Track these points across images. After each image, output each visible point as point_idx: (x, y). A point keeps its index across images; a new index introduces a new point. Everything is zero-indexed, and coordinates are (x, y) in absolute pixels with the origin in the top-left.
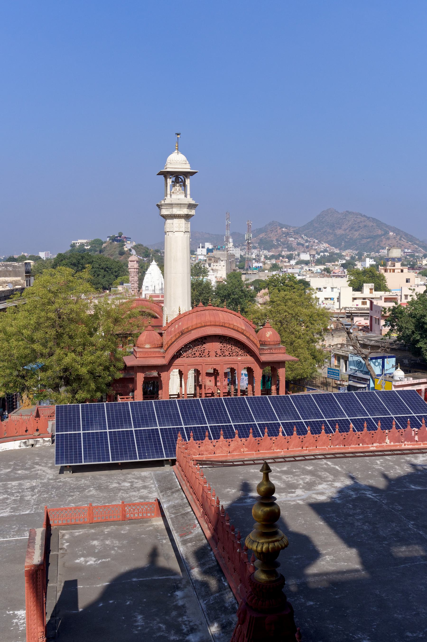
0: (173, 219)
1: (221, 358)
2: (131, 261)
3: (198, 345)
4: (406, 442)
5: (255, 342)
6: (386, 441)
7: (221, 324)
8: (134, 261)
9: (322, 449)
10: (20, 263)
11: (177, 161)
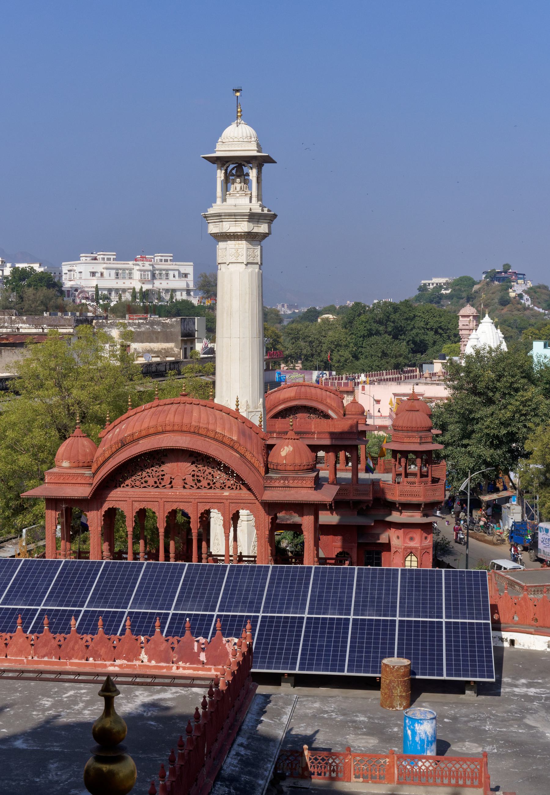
0: (226, 241)
1: (194, 491)
2: (463, 316)
3: (152, 466)
4: (180, 663)
5: (256, 464)
6: (141, 657)
7: (192, 430)
8: (468, 316)
9: (16, 661)
10: (174, 319)
11: (238, 139)
